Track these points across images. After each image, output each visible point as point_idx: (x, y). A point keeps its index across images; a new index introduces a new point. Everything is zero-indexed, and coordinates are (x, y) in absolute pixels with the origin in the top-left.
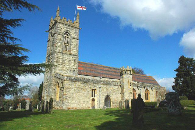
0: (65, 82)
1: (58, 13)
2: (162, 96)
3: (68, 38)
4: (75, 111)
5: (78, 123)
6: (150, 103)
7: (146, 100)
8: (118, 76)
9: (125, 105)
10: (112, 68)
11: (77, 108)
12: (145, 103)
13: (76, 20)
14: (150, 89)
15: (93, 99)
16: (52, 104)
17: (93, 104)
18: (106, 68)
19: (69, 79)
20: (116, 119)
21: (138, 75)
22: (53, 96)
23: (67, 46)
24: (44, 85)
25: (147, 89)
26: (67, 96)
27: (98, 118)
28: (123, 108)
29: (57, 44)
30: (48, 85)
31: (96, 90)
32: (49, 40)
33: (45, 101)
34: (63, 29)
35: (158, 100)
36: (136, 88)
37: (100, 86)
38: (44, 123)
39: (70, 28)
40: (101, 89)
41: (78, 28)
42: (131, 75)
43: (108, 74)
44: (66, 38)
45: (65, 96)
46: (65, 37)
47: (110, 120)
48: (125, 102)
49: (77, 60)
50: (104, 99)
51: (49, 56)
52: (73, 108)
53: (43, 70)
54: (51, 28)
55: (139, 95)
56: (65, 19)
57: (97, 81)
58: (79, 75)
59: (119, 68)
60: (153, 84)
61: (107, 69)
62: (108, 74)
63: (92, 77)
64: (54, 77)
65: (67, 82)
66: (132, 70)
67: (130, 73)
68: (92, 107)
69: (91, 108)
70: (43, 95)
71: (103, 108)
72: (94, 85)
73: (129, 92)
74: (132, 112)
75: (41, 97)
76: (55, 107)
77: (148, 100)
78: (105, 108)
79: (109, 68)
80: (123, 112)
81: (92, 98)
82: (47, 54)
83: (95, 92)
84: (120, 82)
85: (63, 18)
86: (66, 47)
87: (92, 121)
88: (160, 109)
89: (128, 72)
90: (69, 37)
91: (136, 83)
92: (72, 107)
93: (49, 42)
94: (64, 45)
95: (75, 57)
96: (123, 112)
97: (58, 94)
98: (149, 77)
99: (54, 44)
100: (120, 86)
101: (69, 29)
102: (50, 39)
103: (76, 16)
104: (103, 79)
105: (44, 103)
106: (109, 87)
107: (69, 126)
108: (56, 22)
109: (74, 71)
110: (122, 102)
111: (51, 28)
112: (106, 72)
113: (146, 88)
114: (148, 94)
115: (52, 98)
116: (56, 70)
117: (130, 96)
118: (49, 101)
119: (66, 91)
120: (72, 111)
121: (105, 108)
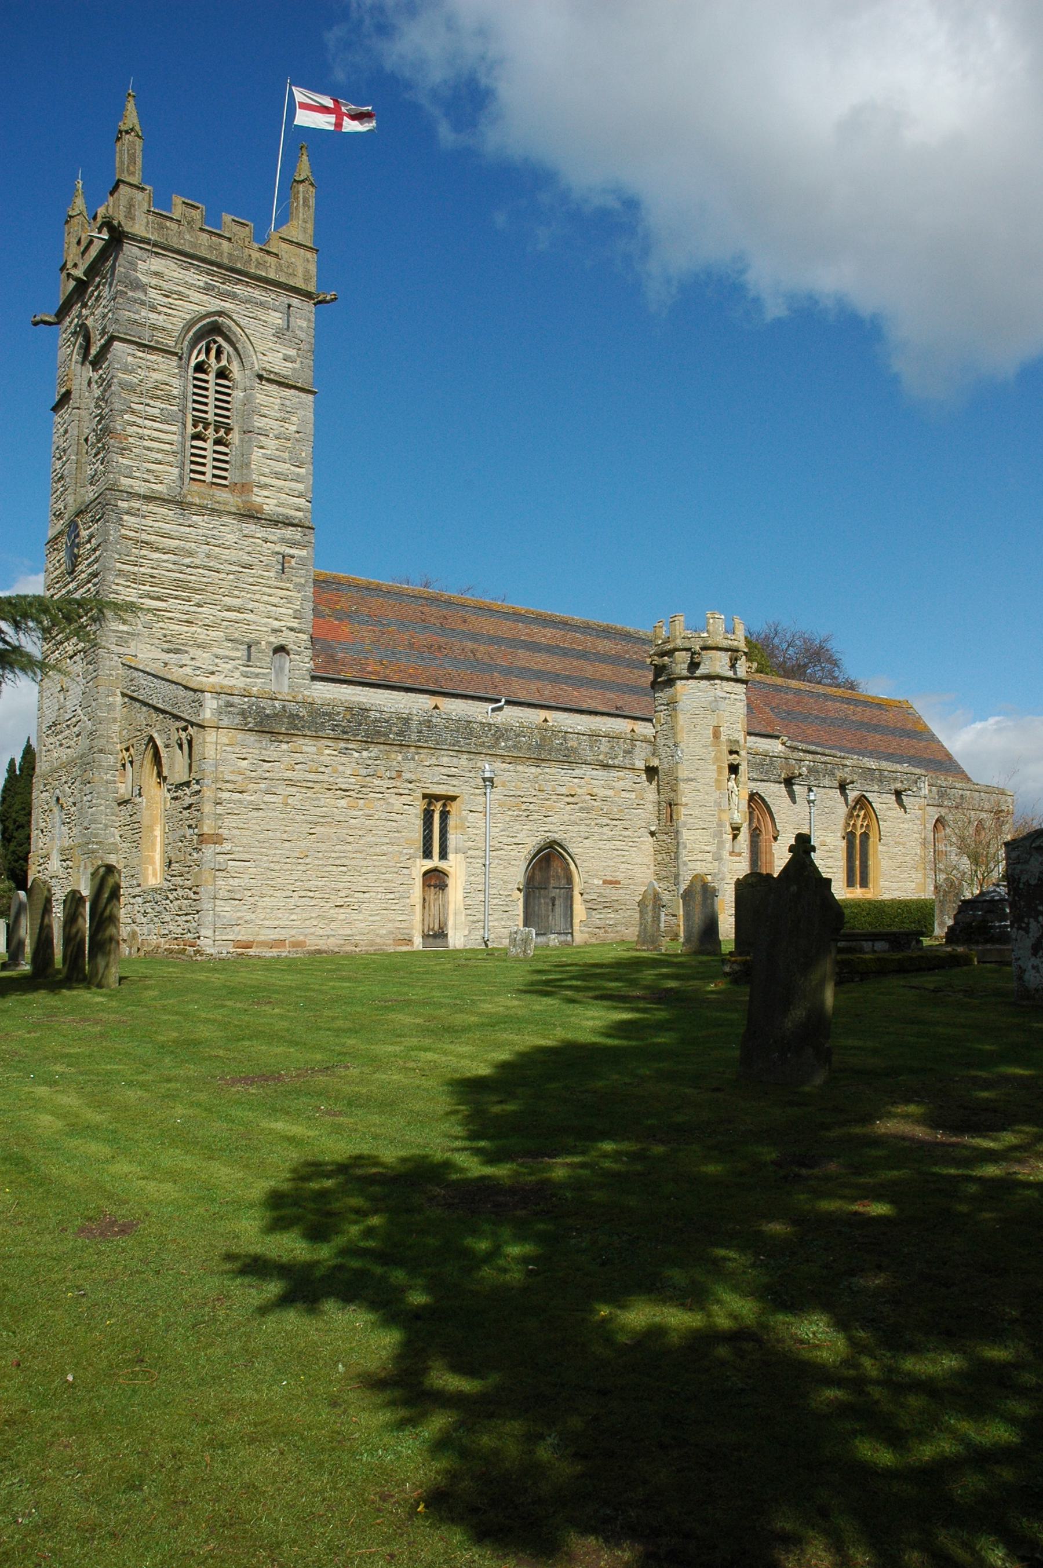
0: (211, 736)
1: (132, 158)
2: (975, 859)
3: (222, 374)
4: (291, 965)
5: (319, 1057)
6: (878, 909)
7: (850, 883)
8: (633, 690)
9: (688, 916)
10: (586, 628)
11: (314, 943)
12: (847, 911)
13: (284, 219)
14: (882, 802)
15: (435, 870)
16: (113, 919)
17: (434, 910)
18: (535, 629)
19: (243, 713)
20: (621, 1029)
21: (794, 684)
22: (116, 850)
23: (218, 442)
24: (42, 767)
25: (862, 802)
26: (227, 846)
27: (474, 1019)
28: (666, 946)
29: (132, 430)
30: (71, 763)
31: (453, 798)
32: (66, 396)
33: (59, 894)
34: (182, 296)
35: (947, 889)
36: (774, 793)
37: (488, 768)
38: (58, 1057)
39: (240, 290)
40: (495, 795)
41: (308, 295)
42: (741, 688)
43: (555, 678)
44: (211, 377)
45: (209, 850)
46: (200, 368)
47: (570, 1036)
48: (687, 895)
49: (303, 562)
50: (517, 874)
51: (73, 527)
52: (281, 943)
53: (31, 644)
54: (819, 787)
55: (803, 846)
56: (196, 214)
57: (466, 727)
58: (319, 685)
59: (644, 630)
60: (914, 760)
61: (549, 632)
62: (555, 678)
63: (425, 702)
64: (119, 699)
65: (224, 736)
66: (748, 642)
67: (733, 666)
68: (425, 936)
69: (418, 942)
70: (38, 842)
71: (513, 942)
72: (445, 760)
73: (720, 825)
74: (736, 979)
75: (26, 859)
76: (134, 934)
77: (864, 884)
78: (526, 941)
79: (564, 624)
80: (667, 977)
81: (429, 864)
82: (59, 516)
83: (452, 822)
84: (652, 742)
85: (178, 200)
86: (209, 453)
87: (427, 1042)
88: (965, 960)
89: (719, 663)
90: (235, 367)
91: (776, 747)
92: (274, 935)
93: (65, 413)
94: (196, 437)
95: (283, 540)
96: (667, 977)
97: (158, 832)
98: (880, 705)
99: (107, 431)
100: (651, 772)
101: (233, 296)
102: (75, 387)
103: (291, 183)
104: (511, 715)
105: (47, 909)
106: (556, 775)
107: (249, 1080)
108: (117, 238)
109: (281, 649)
110: (666, 897)
111: (82, 286)
112: (538, 661)
113: (852, 795)
114: (865, 836)
115: (110, 869)
116: (133, 648)
117: (725, 854)
118: (85, 892)
119: (220, 809)
120: (269, 965)
121: (526, 941)
